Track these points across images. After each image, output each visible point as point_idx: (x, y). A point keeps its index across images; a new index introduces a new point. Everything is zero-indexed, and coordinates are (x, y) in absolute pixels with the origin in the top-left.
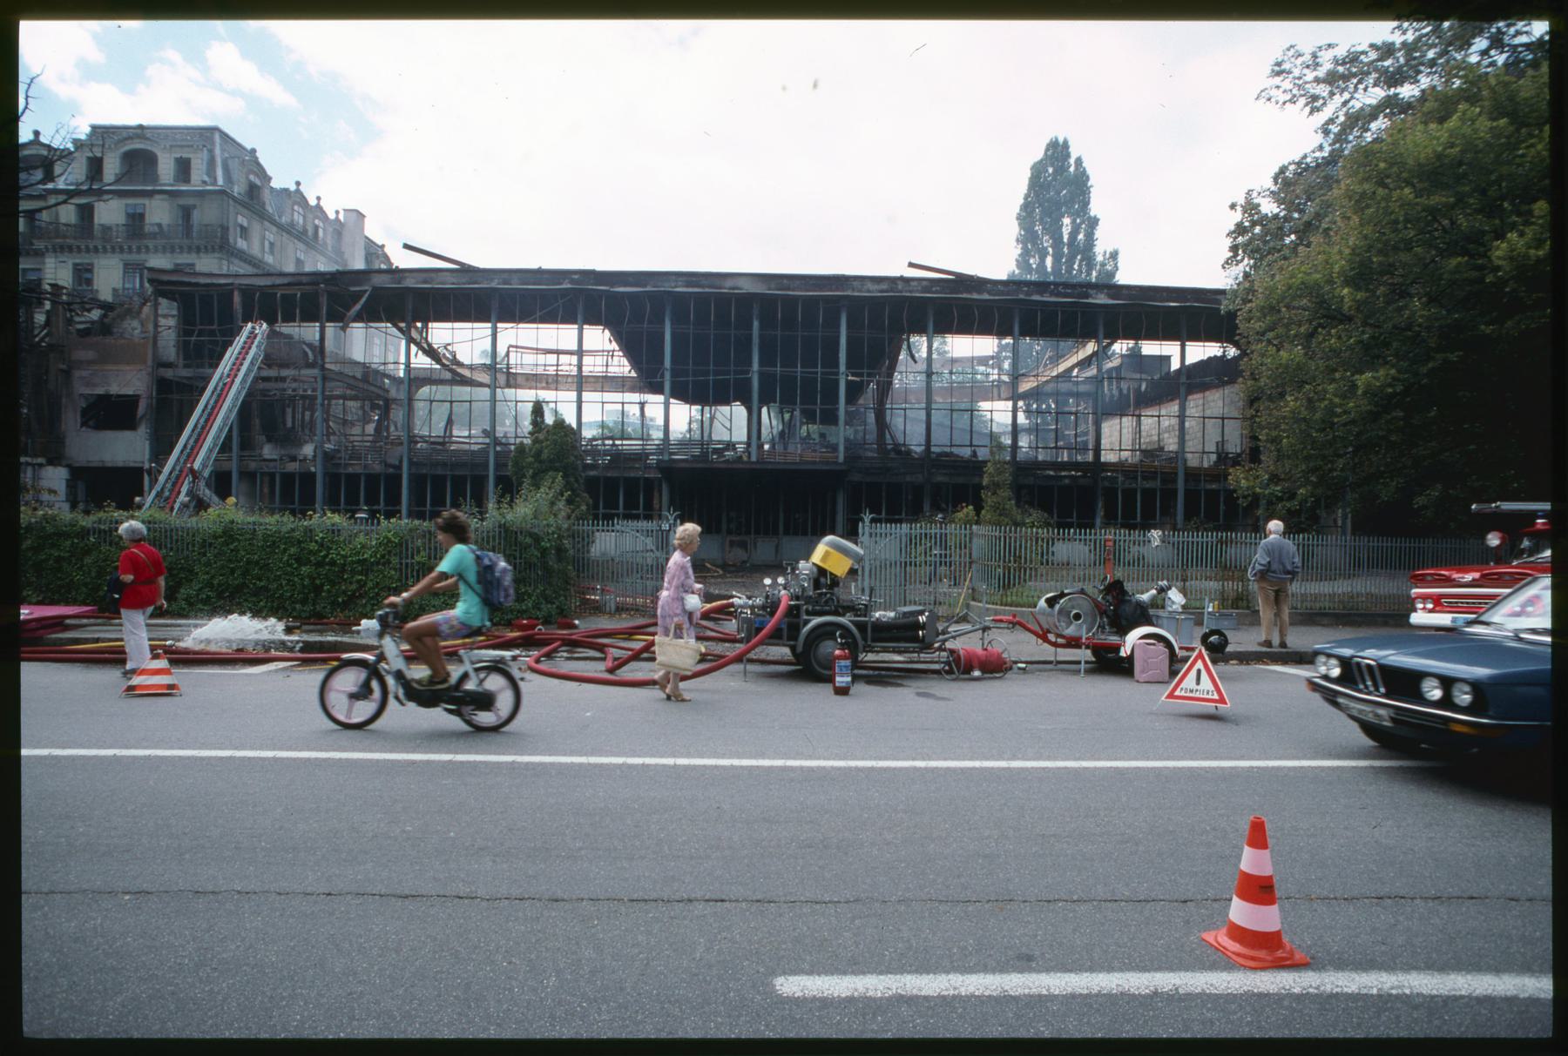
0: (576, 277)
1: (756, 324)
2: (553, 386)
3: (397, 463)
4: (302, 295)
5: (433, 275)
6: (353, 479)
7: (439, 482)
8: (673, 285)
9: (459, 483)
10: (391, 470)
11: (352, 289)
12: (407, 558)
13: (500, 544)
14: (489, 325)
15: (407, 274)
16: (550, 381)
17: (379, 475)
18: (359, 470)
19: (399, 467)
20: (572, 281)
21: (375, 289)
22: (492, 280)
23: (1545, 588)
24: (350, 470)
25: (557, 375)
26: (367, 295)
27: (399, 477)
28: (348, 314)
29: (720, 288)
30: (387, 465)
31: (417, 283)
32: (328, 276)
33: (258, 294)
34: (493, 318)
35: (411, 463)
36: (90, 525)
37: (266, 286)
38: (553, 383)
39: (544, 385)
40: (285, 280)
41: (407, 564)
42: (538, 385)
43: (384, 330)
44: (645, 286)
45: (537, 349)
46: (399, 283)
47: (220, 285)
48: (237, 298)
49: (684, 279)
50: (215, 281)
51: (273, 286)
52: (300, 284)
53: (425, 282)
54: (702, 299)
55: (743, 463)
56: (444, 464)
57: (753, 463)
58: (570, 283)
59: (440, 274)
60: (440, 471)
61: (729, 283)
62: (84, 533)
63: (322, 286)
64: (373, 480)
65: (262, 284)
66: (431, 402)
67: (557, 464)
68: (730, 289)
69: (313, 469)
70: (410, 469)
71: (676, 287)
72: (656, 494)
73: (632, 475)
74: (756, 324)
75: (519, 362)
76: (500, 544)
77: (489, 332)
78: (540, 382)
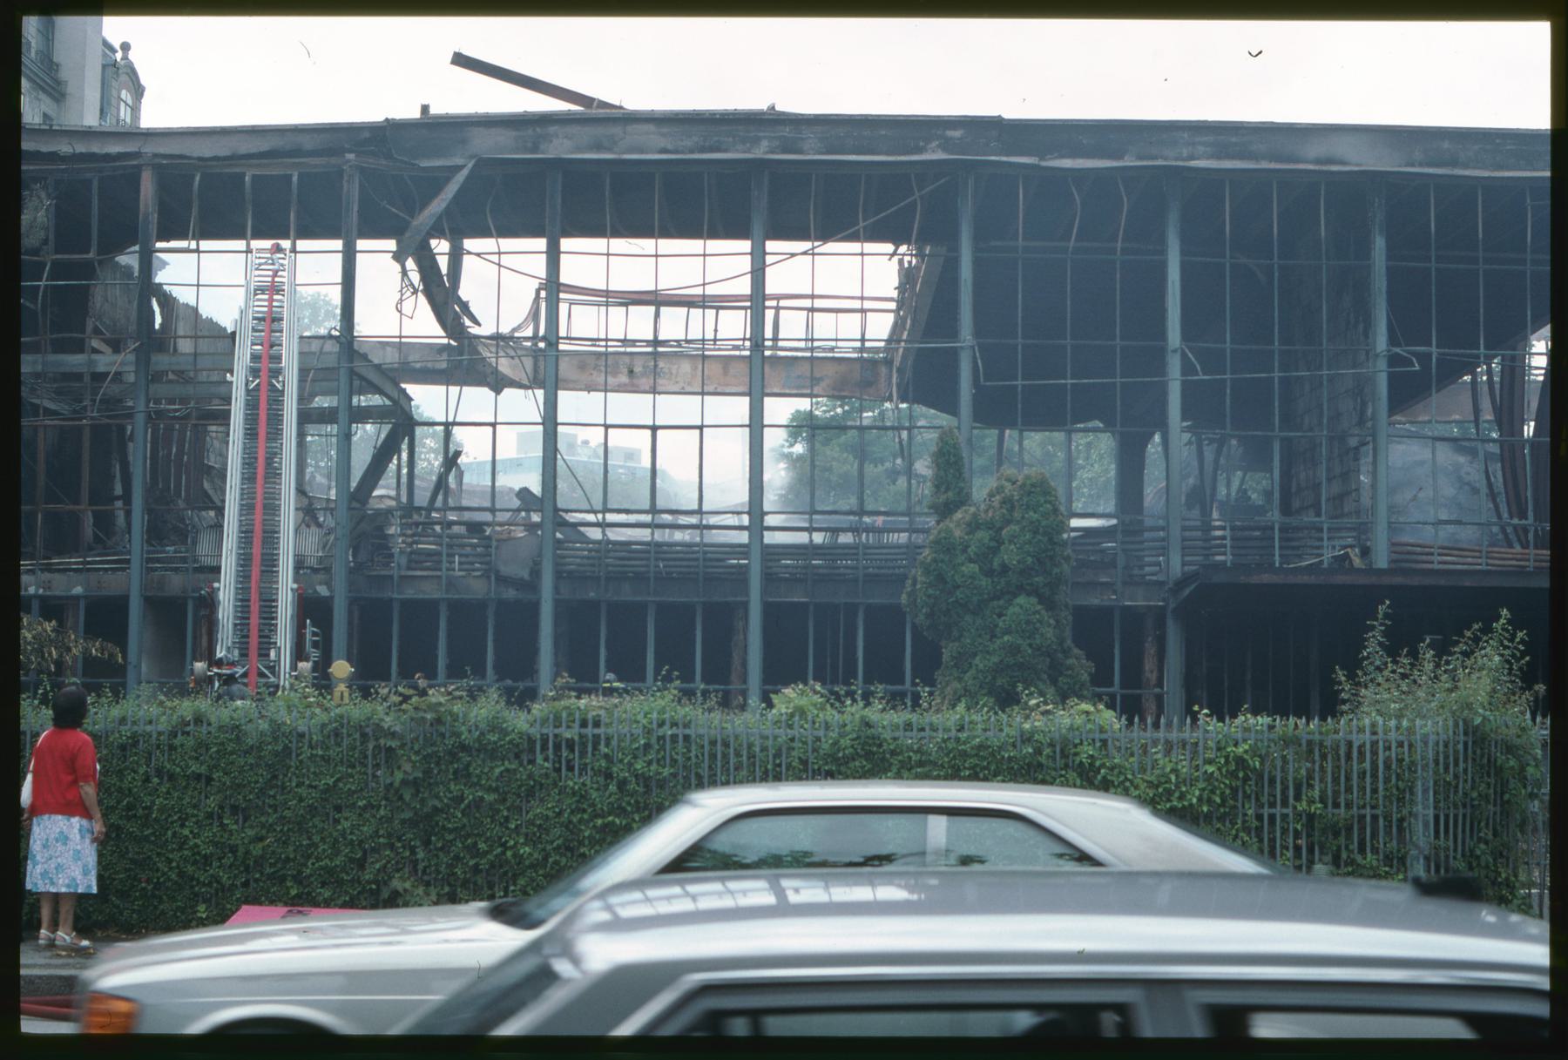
0: (957, 134)
1: (1380, 243)
2: (645, 382)
3: (525, 574)
4: (301, 175)
5: (616, 130)
6: (420, 614)
7: (627, 619)
8: (1185, 152)
9: (675, 621)
10: (510, 594)
11: (425, 163)
12: (1272, 805)
13: (1465, 770)
14: (745, 245)
15: (552, 129)
16: (638, 369)
17: (482, 605)
18: (430, 591)
19: (532, 585)
20: (947, 145)
21: (482, 163)
22: (757, 140)
23: (89, 887)
24: (410, 593)
25: (655, 354)
26: (461, 177)
27: (535, 608)
28: (415, 223)
29: (1298, 161)
30: (503, 580)
31: (579, 149)
32: (367, 135)
33: (198, 178)
34: (757, 227)
35: (559, 575)
36: (535, 732)
37: (216, 158)
38: (644, 374)
39: (624, 379)
40: (263, 145)
41: (1272, 818)
42: (611, 380)
43: (495, 258)
44: (1121, 158)
45: (607, 293)
46: (535, 149)
47: (107, 157)
48: (148, 187)
49: (1210, 138)
50: (96, 148)
51: (234, 158)
52: (296, 152)
53: (598, 147)
54: (1253, 189)
55: (1353, 570)
56: (640, 578)
57: (1381, 572)
58: (945, 150)
59: (629, 128)
60: (627, 594)
61: (1315, 149)
62: (525, 748)
63: (351, 156)
64: (466, 614)
65: (207, 154)
66: (654, 429)
67: (1038, 579)
68: (1318, 161)
69: (323, 591)
70: (556, 590)
71: (1192, 158)
72: (1150, 649)
73: (1095, 601)
74: (1380, 243)
75: (710, 335)
76: (1465, 770)
77: (745, 264)
78: (615, 374)
